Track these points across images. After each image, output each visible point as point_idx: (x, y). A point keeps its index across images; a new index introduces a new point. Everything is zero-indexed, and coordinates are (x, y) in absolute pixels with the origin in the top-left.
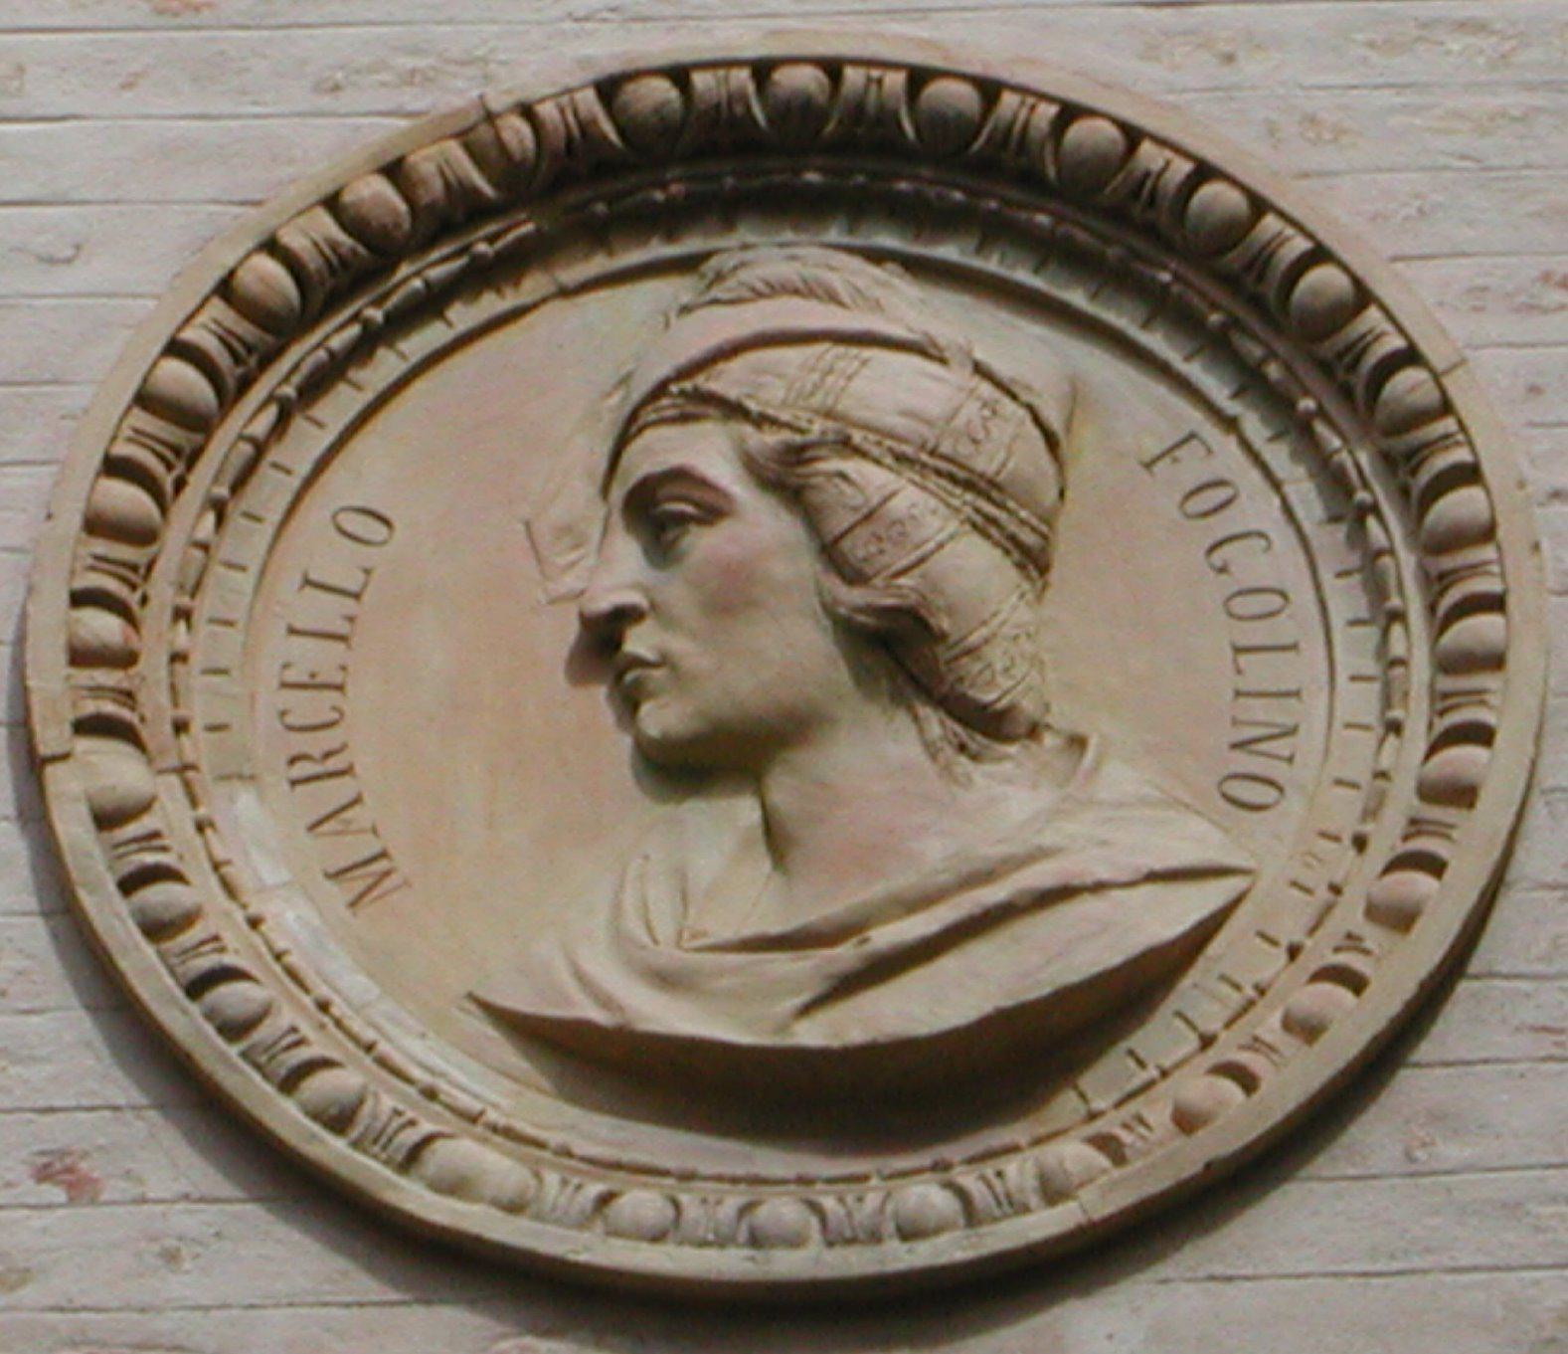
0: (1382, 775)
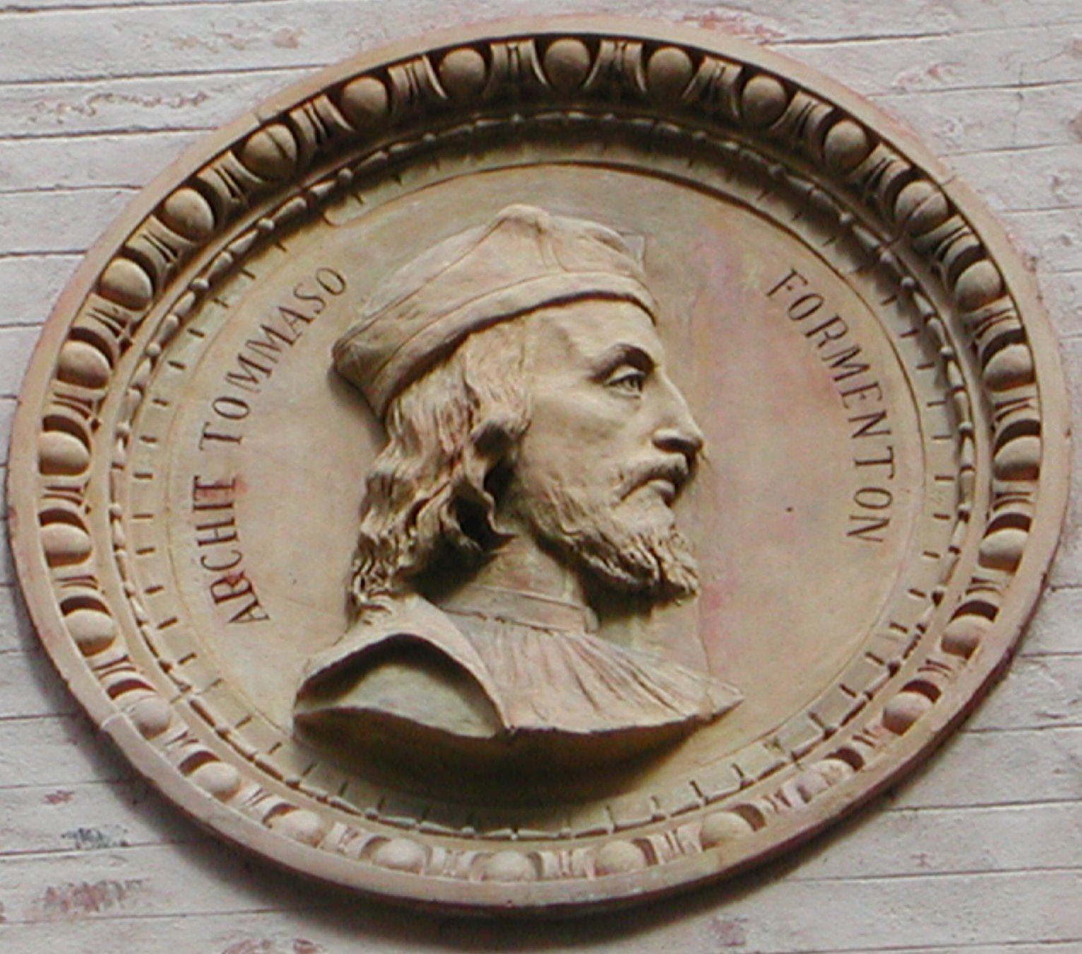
0: (955, 550)
